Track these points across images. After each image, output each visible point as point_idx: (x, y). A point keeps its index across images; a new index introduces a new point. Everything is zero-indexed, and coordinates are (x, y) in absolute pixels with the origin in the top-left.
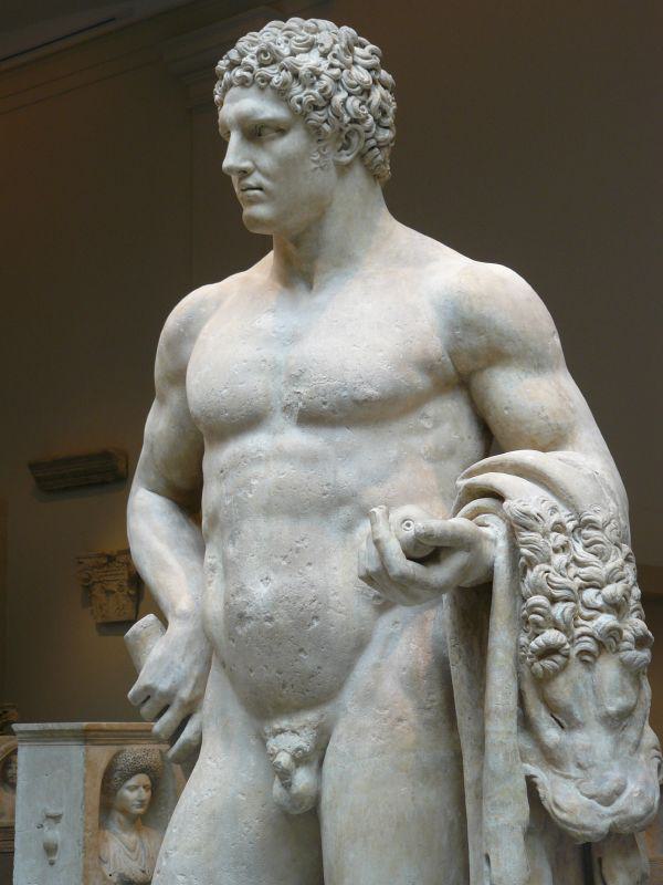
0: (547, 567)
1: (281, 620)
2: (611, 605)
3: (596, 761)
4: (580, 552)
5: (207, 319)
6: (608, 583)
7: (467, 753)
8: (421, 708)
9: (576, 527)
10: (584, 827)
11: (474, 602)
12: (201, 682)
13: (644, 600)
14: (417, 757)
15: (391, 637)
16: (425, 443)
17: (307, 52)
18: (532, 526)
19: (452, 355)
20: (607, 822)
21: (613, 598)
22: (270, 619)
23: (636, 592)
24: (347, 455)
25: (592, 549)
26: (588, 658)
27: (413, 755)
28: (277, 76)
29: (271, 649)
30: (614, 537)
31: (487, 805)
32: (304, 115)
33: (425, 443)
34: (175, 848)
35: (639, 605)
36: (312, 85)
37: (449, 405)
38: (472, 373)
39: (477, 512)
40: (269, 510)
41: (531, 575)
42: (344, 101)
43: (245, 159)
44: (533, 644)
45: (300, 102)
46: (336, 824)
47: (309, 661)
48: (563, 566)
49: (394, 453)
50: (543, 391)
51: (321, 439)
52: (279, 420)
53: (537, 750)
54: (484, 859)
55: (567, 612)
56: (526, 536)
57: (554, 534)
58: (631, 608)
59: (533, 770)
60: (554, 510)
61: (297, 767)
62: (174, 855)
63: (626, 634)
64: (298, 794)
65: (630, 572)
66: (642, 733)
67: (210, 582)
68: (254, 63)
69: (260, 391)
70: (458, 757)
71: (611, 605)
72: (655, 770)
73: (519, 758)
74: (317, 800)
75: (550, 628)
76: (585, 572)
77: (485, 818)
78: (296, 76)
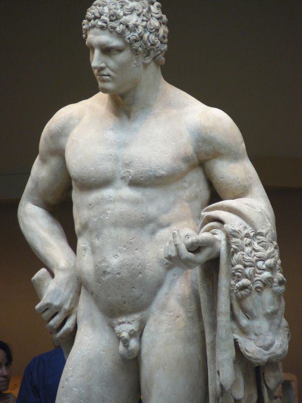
0: (242, 253)
1: (125, 273)
2: (269, 268)
3: (263, 332)
4: (257, 246)
5: (74, 127)
6: (268, 259)
7: (207, 330)
8: (187, 312)
9: (254, 235)
10: (257, 359)
11: (211, 268)
12: (75, 301)
13: (282, 265)
14: (185, 333)
15: (173, 281)
16: (187, 193)
17: (130, 14)
18: (237, 236)
19: (196, 153)
20: (267, 357)
21: (270, 265)
22: (119, 274)
23: (279, 261)
24: (151, 200)
25: (261, 244)
26: (259, 290)
27: (183, 332)
28: (119, 28)
29: (119, 287)
30: (270, 239)
31: (218, 351)
32: (131, 44)
33: (187, 193)
34: (72, 376)
35: (280, 267)
36: (135, 31)
37: (195, 175)
38: (206, 161)
39: (212, 228)
40: (115, 225)
41: (236, 256)
42: (148, 37)
43: (102, 63)
44: (237, 285)
45: (129, 38)
46: (149, 363)
47: (137, 292)
48: (249, 252)
49: (172, 199)
50: (239, 170)
51: (140, 193)
52: (119, 183)
53: (238, 328)
54: (217, 372)
55: (251, 271)
56: (234, 240)
57: (246, 239)
58: (277, 269)
59: (236, 336)
60: (245, 228)
61: (131, 338)
62: (71, 379)
63: (275, 280)
64: (132, 350)
65: (277, 253)
66: (281, 322)
67: (84, 256)
68: (107, 19)
69: (110, 170)
70: (203, 333)
71: (269, 268)
72: (286, 336)
73: (231, 332)
74: (139, 352)
75: (244, 278)
76: (258, 254)
77: (217, 356)
78: (127, 26)
